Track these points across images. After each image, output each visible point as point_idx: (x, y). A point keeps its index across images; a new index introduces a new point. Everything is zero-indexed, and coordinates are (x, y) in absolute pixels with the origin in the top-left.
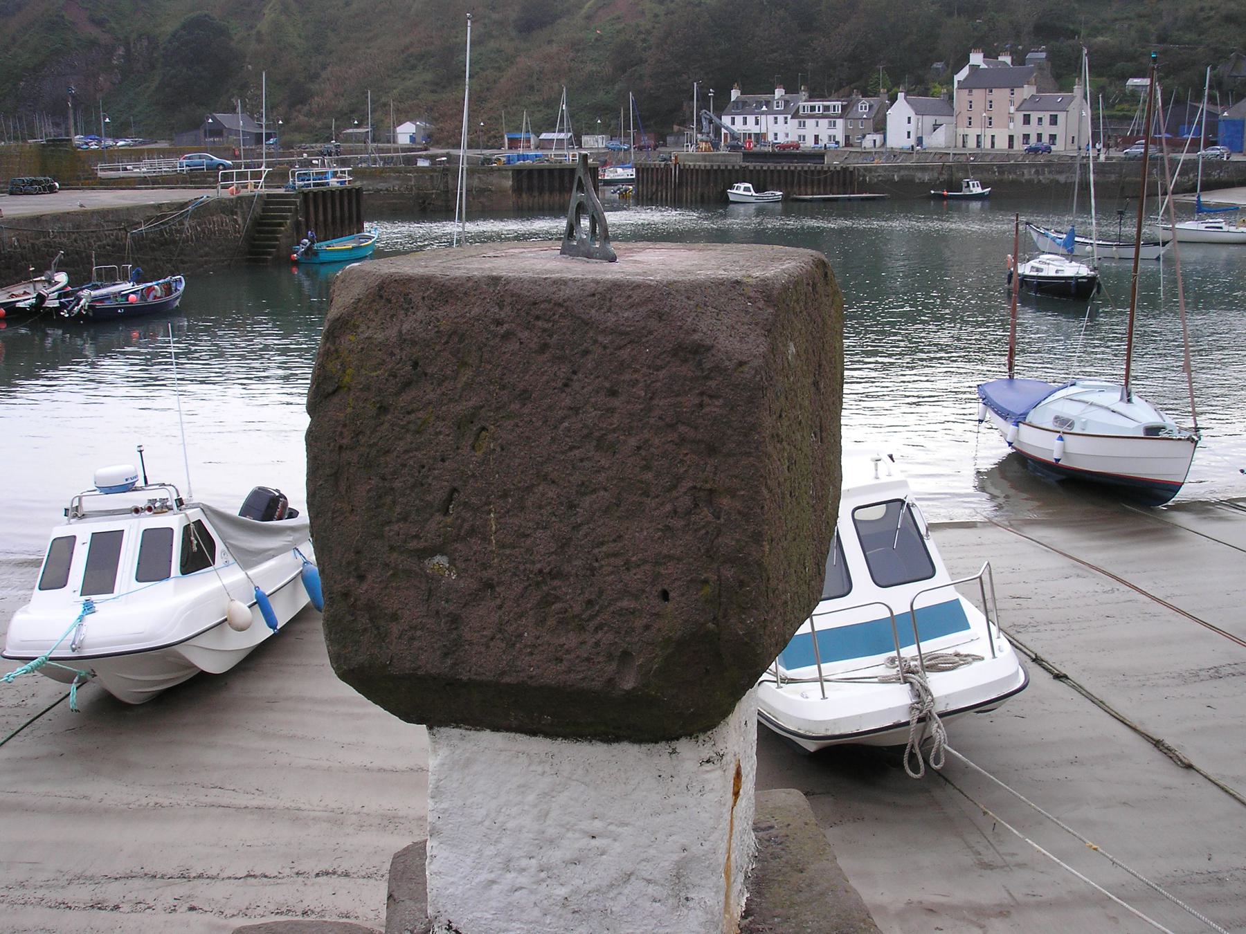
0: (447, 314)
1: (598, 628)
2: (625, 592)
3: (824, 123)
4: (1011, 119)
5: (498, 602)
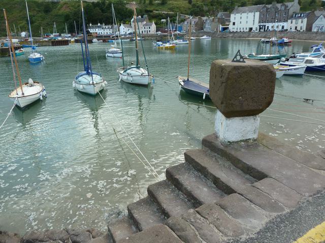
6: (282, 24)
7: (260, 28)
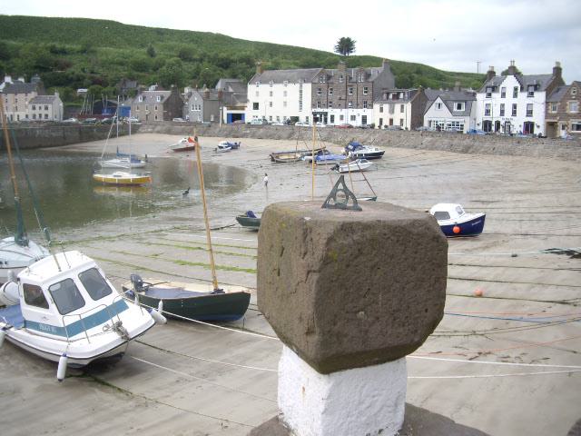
2: (417, 312)
4: (26, 107)
6: (360, 112)
7: (316, 120)
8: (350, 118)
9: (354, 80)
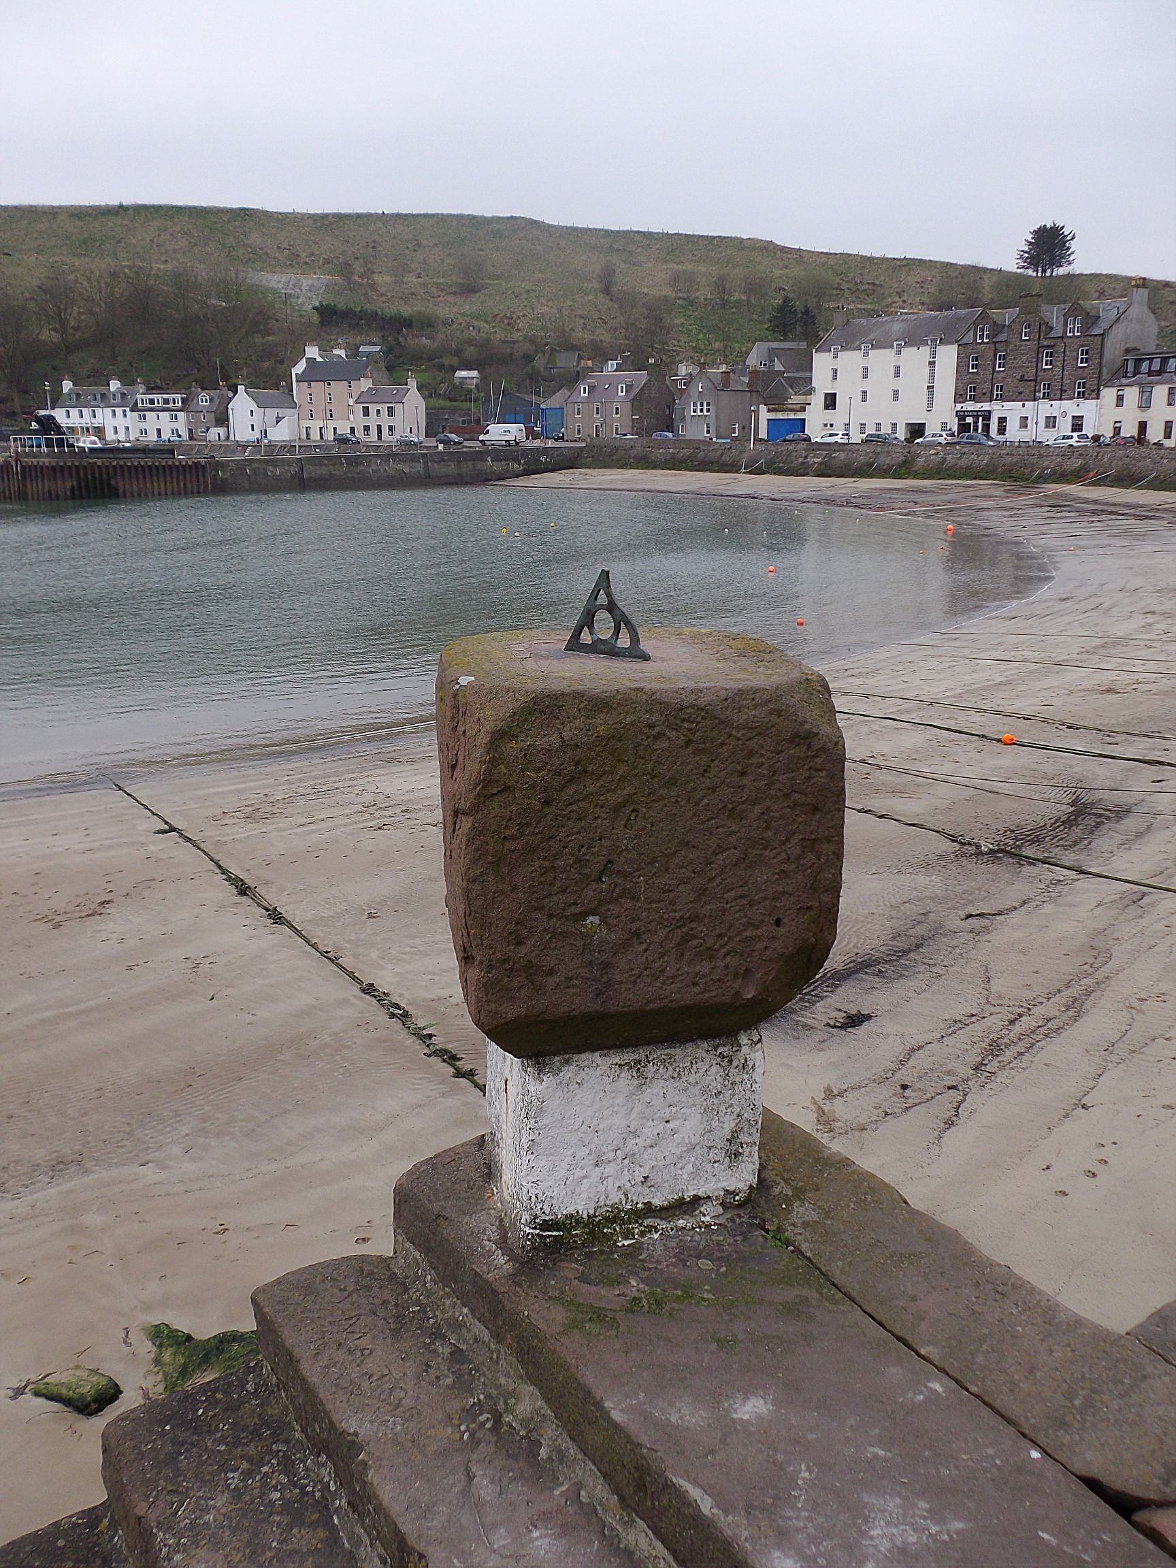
0: (603, 724)
1: (727, 954)
3: (165, 416)
5: (644, 946)
6: (1070, 407)
8: (1042, 422)
9: (1057, 332)
